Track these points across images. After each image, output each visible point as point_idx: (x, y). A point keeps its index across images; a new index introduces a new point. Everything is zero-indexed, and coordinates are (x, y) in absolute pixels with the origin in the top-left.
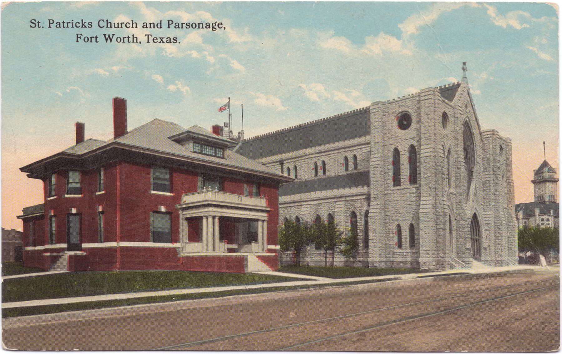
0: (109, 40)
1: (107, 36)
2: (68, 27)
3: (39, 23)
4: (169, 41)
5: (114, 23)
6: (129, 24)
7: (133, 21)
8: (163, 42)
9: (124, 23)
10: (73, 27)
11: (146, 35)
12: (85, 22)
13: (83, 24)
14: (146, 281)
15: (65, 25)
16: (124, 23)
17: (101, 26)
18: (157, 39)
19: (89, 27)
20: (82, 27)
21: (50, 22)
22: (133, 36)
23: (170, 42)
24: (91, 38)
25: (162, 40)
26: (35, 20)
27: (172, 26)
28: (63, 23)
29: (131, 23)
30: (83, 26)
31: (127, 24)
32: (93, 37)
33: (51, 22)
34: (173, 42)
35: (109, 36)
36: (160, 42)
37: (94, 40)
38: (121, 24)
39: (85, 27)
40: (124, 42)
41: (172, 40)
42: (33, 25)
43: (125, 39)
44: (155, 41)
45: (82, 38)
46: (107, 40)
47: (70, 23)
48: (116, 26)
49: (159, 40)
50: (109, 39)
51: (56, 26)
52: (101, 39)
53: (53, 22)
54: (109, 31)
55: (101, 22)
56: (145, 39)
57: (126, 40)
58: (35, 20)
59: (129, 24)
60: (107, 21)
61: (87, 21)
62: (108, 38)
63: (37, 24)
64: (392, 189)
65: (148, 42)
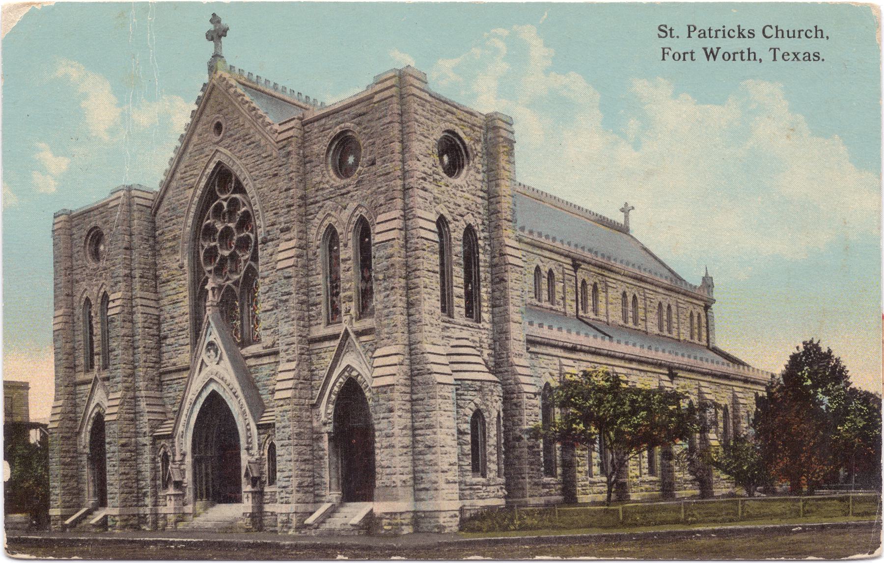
0: (711, 57)
1: (709, 51)
2: (716, 37)
3: (671, 30)
4: (808, 57)
5: (788, 31)
6: (811, 31)
7: (816, 27)
8: (798, 60)
9: (803, 30)
10: (724, 37)
11: (771, 49)
12: (743, 30)
13: (739, 33)
14: (531, 464)
15: (713, 33)
16: (803, 30)
17: (767, 34)
18: (788, 55)
19: (749, 37)
20: (739, 37)
21: (689, 28)
22: (749, 49)
23: (809, 60)
24: (734, 54)
25: (796, 56)
26: (666, 26)
27: (694, 35)
28: (710, 30)
29: (814, 31)
30: (741, 34)
31: (731, 31)
32: (687, 53)
33: (691, 29)
34: (814, 60)
35: (712, 52)
36: (793, 60)
37: (688, 56)
38: (799, 32)
39: (744, 37)
40: (734, 60)
41: (812, 57)
42: (663, 34)
43: (686, 55)
44: (786, 57)
45: (671, 54)
46: (708, 57)
47: (720, 30)
48: (791, 34)
49: (792, 56)
50: (711, 56)
51: (699, 36)
52: (700, 55)
53: (695, 29)
54: (711, 44)
55: (768, 30)
56: (768, 56)
57: (738, 56)
58: (666, 26)
59: (811, 31)
60: (777, 27)
61: (746, 27)
62: (711, 54)
63: (669, 32)
64: (293, 174)
65: (775, 59)
